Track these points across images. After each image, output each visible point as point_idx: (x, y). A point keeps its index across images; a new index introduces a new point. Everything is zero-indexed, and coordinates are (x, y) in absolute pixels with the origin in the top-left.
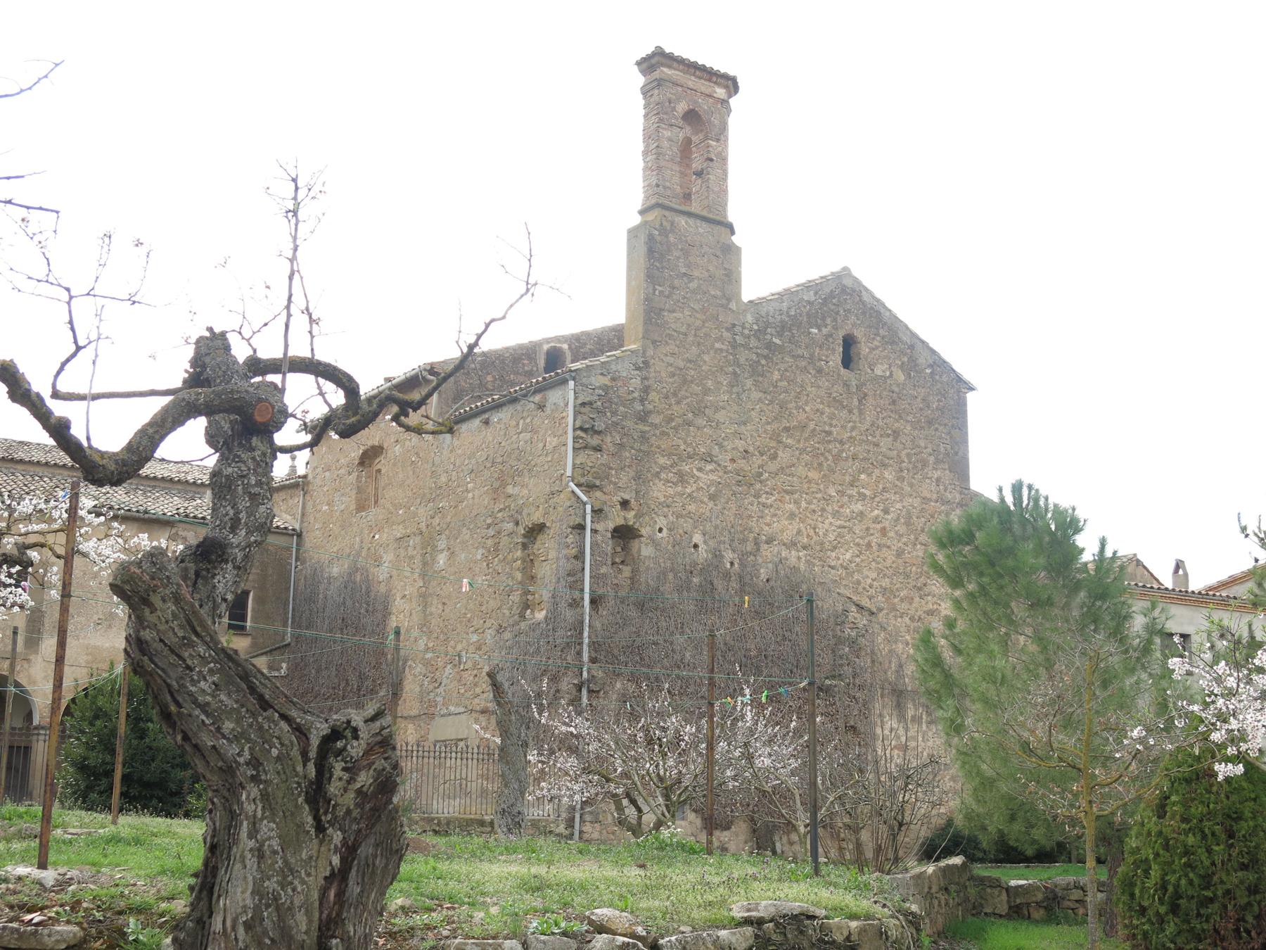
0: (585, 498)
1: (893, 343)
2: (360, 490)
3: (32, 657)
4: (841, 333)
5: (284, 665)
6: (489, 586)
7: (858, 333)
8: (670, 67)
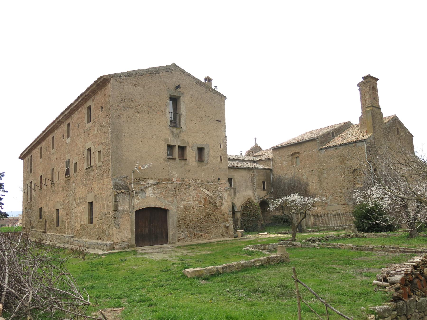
0: (370, 164)
1: (403, 129)
2: (292, 161)
3: (235, 198)
4: (396, 128)
5: (272, 196)
6: (342, 180)
7: (398, 127)
8: (370, 78)
